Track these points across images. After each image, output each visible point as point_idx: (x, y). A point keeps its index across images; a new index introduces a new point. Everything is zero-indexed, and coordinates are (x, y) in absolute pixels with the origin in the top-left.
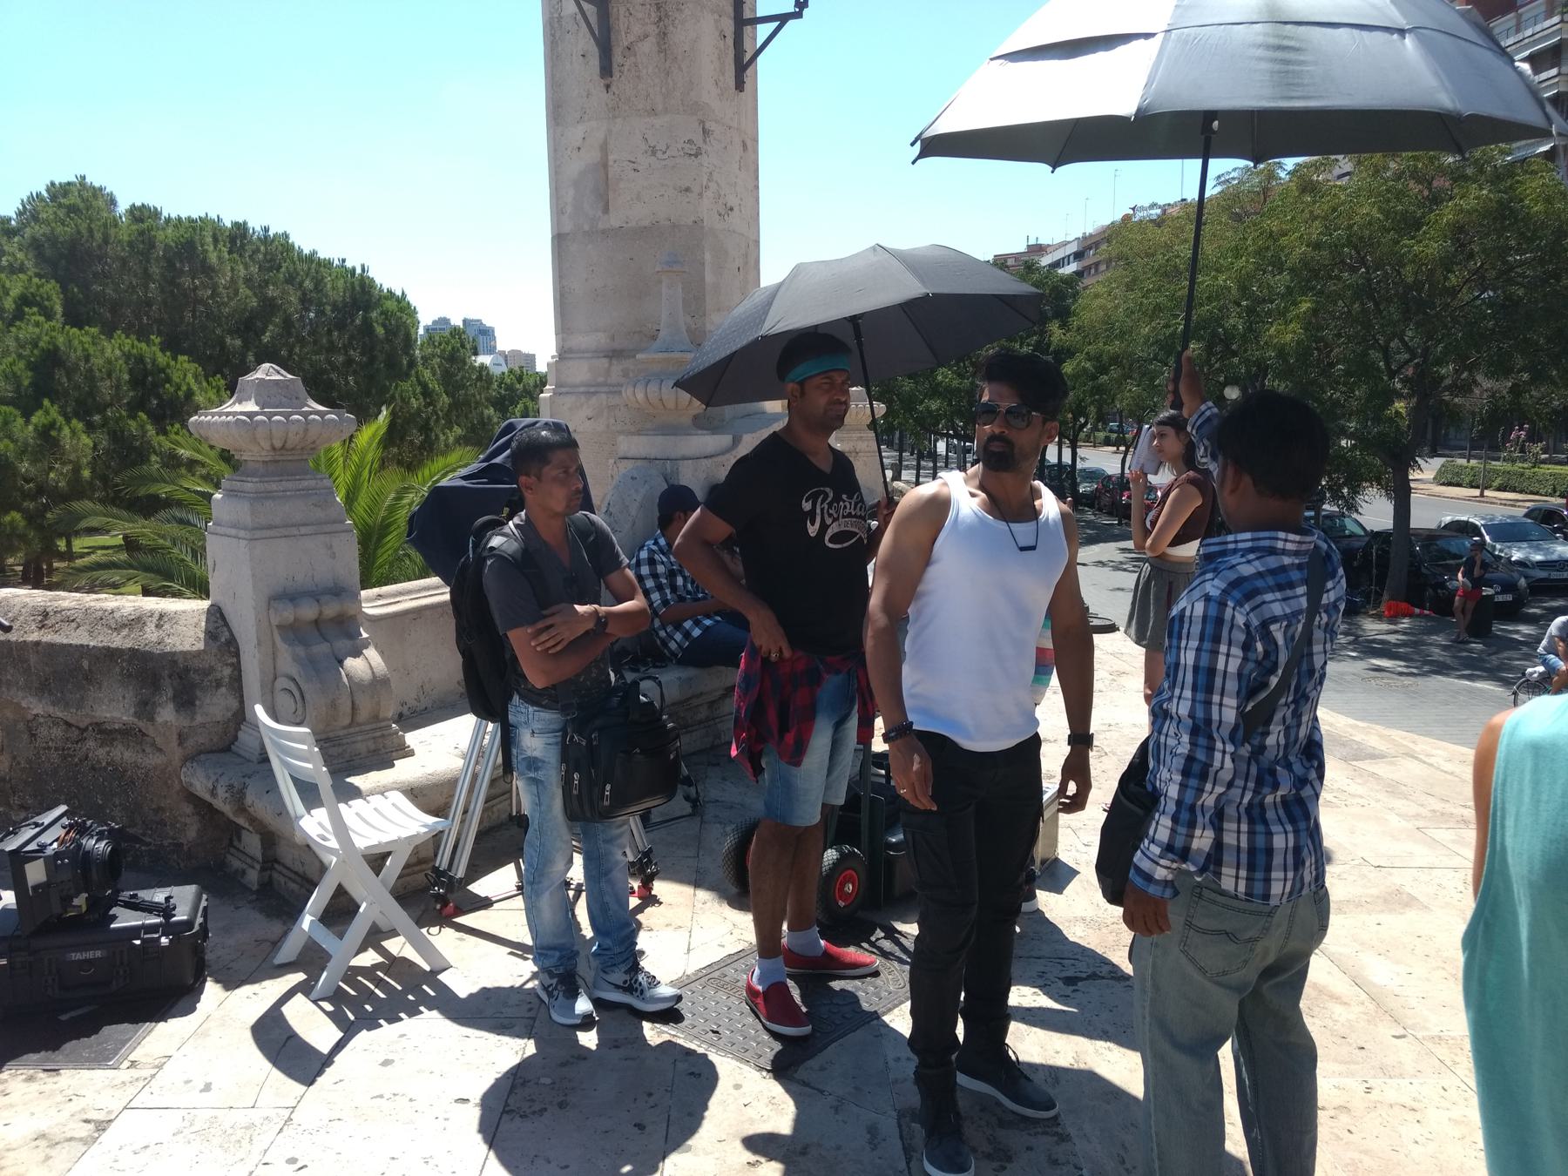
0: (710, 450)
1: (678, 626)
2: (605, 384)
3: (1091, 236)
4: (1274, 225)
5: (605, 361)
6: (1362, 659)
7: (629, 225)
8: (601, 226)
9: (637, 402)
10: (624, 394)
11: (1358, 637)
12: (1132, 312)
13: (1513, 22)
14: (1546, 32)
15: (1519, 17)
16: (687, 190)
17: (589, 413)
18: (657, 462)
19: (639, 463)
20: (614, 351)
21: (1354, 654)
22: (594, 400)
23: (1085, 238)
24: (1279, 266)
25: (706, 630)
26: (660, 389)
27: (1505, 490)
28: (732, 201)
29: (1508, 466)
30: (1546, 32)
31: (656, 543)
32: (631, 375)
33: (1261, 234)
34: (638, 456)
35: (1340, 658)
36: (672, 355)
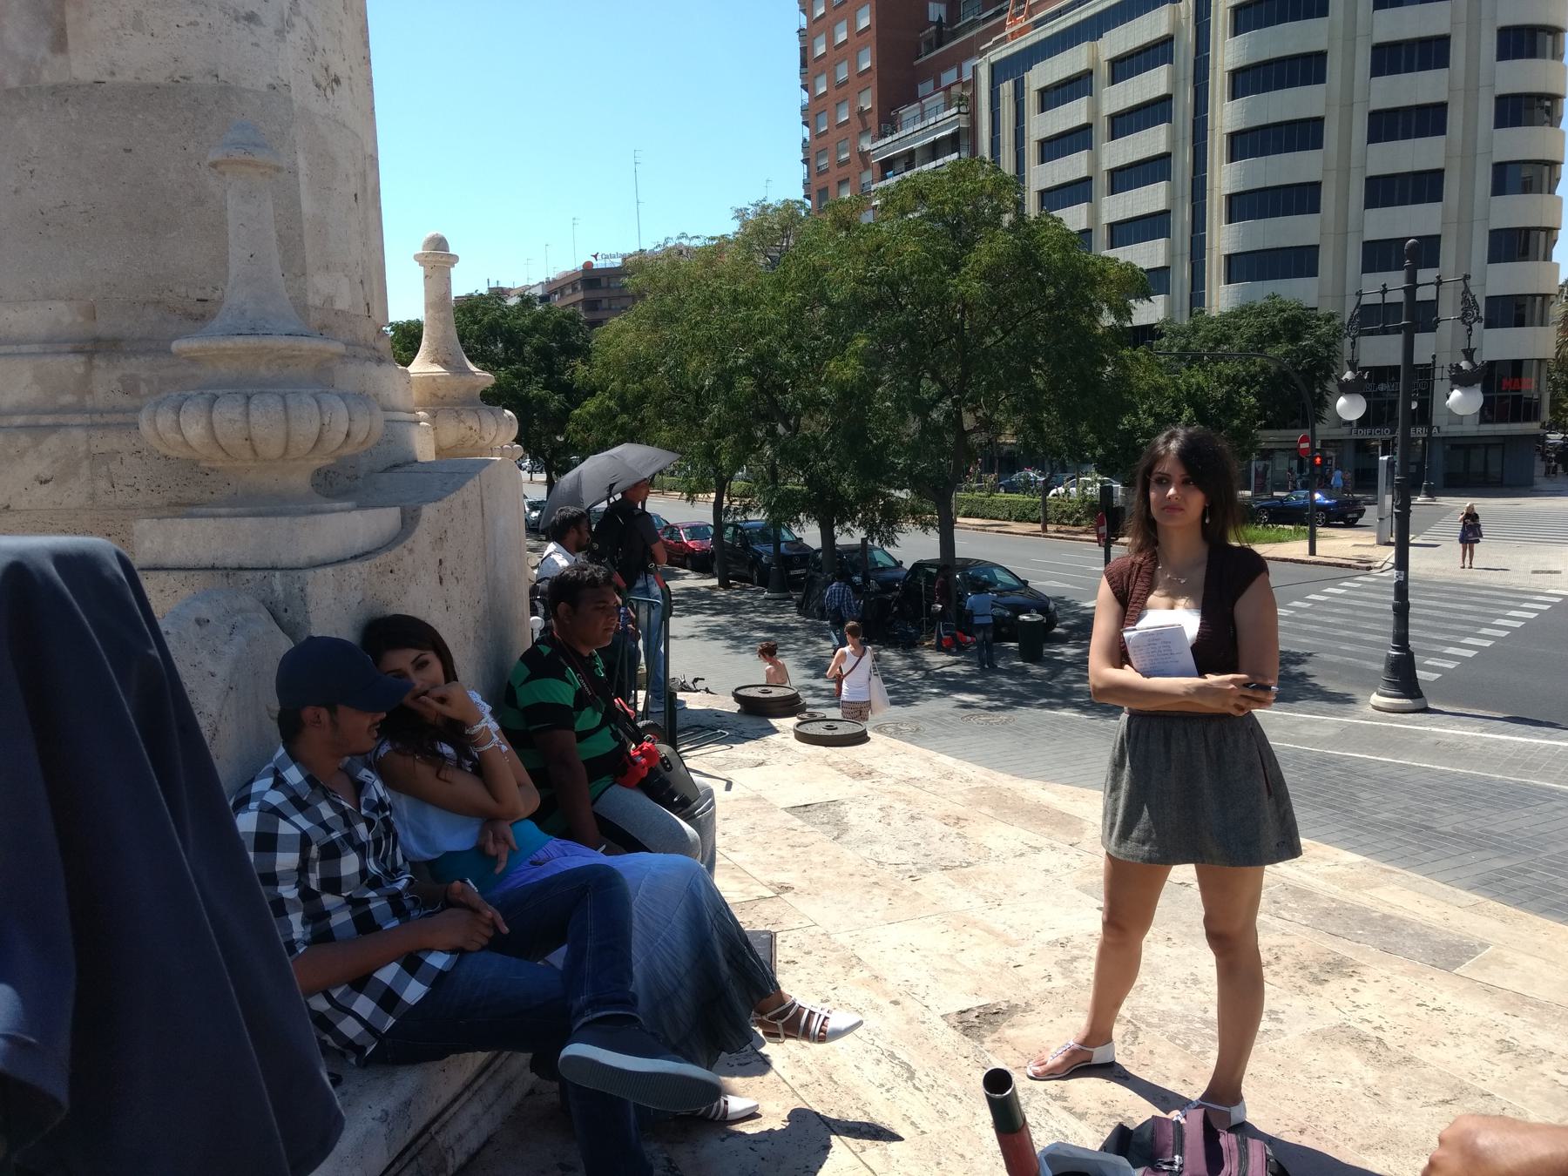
0: (360, 542)
1: (361, 983)
2: (80, 409)
3: (555, 281)
4: (815, 259)
5: (77, 364)
6: (945, 696)
7: (119, 78)
8: (47, 77)
9: (186, 443)
10: (145, 426)
11: (927, 671)
12: (686, 345)
13: (919, 111)
14: (946, 121)
15: (922, 107)
16: (251, 18)
17: (42, 468)
18: (248, 575)
19: (199, 579)
20: (97, 340)
21: (935, 691)
22: (52, 442)
23: (549, 282)
24: (823, 298)
25: (439, 981)
26: (248, 415)
27: (970, 517)
28: (339, 68)
29: (969, 496)
30: (946, 121)
31: (279, 783)
32: (144, 389)
33: (804, 268)
34: (191, 564)
35: (924, 696)
36: (268, 342)
